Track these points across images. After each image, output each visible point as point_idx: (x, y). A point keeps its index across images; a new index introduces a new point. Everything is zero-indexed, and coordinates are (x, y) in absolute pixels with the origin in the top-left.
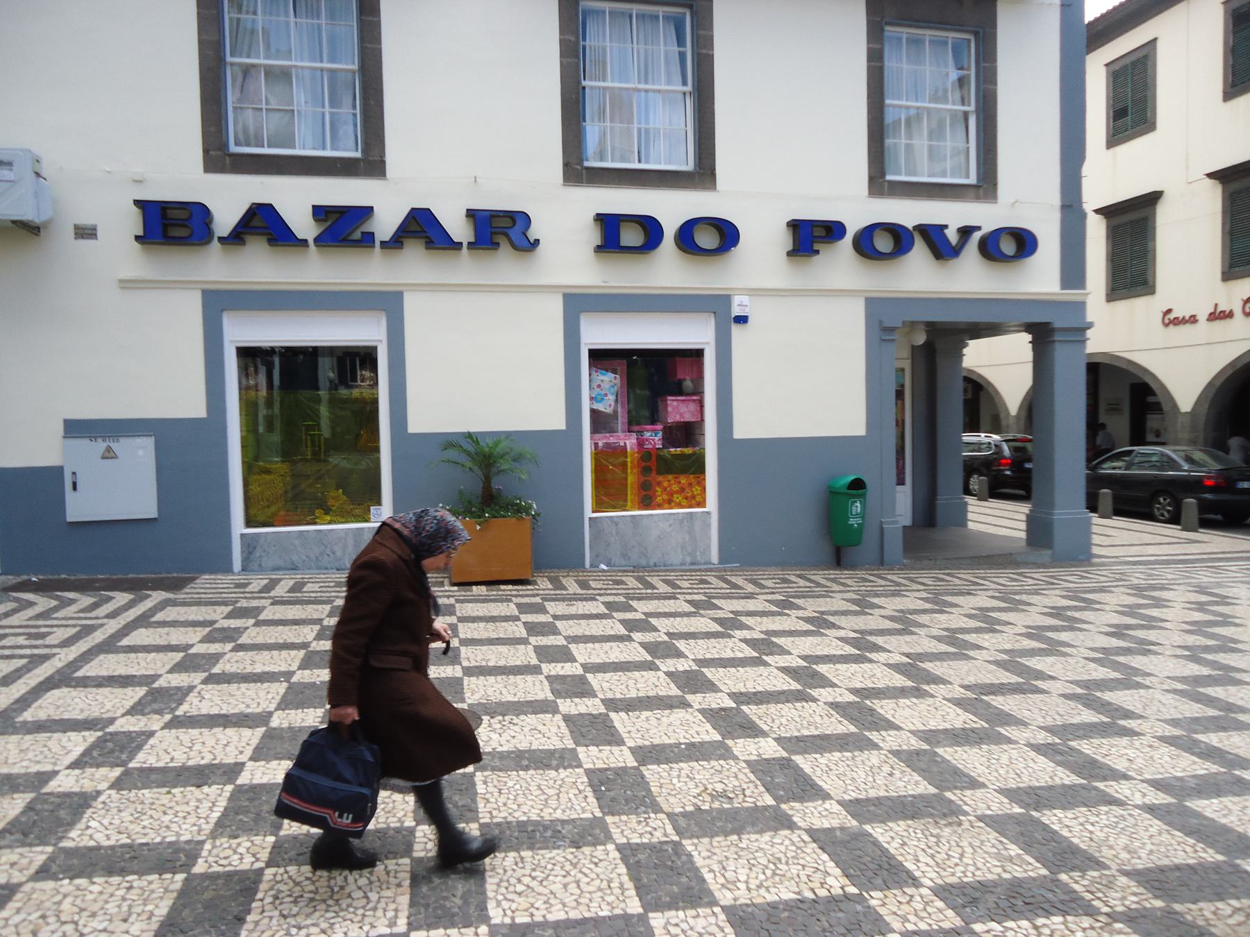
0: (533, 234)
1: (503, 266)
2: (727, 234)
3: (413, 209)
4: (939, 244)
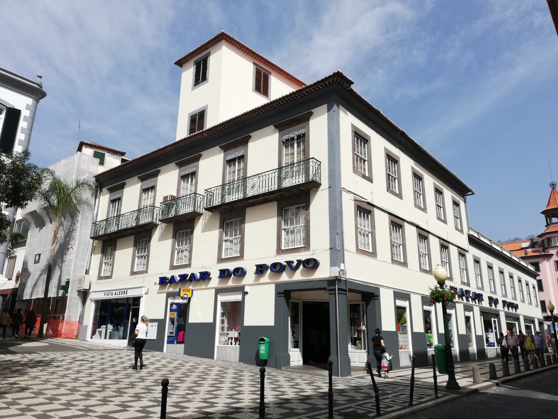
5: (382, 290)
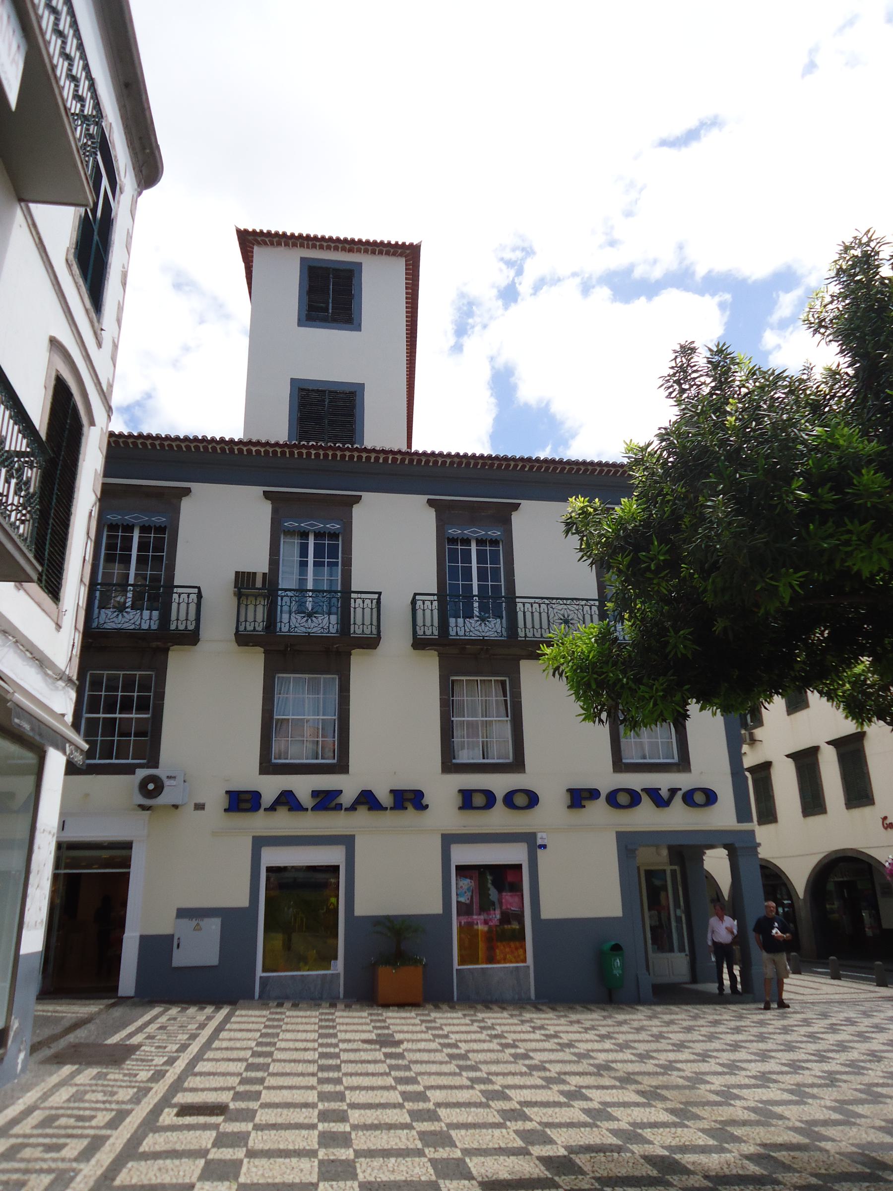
0: (425, 801)
1: (410, 815)
2: (533, 800)
3: (239, 645)
4: (659, 800)
5: (110, 429)
